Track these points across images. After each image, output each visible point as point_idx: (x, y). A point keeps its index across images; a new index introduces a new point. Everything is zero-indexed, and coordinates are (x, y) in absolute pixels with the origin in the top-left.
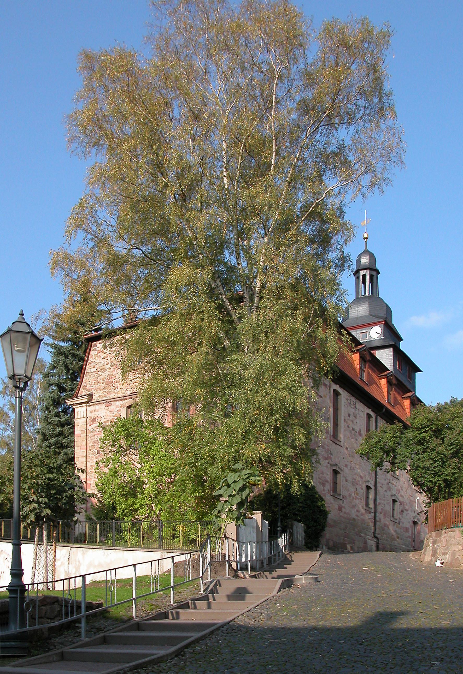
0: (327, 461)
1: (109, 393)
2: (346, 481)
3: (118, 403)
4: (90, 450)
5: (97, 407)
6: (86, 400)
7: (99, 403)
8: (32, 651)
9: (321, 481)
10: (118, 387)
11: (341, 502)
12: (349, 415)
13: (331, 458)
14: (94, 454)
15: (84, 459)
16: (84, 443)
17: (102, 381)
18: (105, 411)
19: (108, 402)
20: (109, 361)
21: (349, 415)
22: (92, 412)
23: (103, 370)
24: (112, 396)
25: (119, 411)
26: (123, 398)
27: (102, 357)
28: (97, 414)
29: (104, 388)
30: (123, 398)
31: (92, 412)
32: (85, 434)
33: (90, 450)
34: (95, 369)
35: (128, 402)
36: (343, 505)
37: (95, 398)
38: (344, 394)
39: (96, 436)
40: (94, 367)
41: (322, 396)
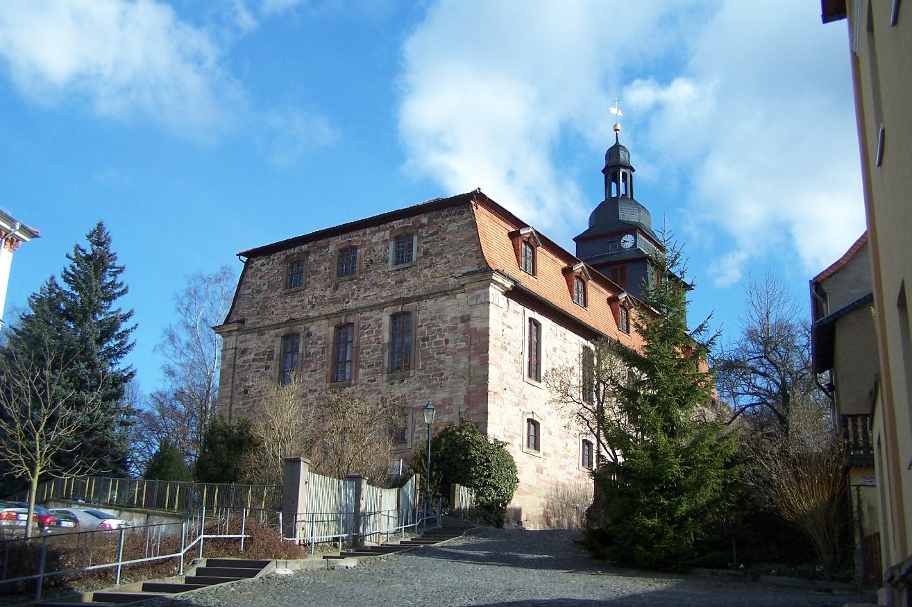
0: (517, 408)
1: (263, 319)
2: (550, 433)
3: (272, 332)
4: (236, 389)
5: (249, 336)
6: (236, 328)
7: (250, 331)
8: (456, 507)
9: (507, 433)
10: (273, 312)
11: (540, 461)
12: (555, 349)
13: (525, 405)
14: (240, 394)
15: (229, 401)
16: (230, 380)
17: (256, 305)
18: (257, 342)
19: (261, 331)
20: (266, 282)
21: (555, 349)
22: (241, 342)
23: (259, 292)
24: (267, 323)
25: (272, 342)
26: (278, 326)
27: (259, 276)
28: (247, 345)
29: (258, 314)
30: (278, 326)
31: (241, 342)
32: (232, 369)
33: (236, 389)
34: (250, 290)
35: (282, 331)
36: (544, 465)
37: (249, 323)
38: (546, 323)
39: (244, 372)
40: (249, 288)
41: (512, 326)
